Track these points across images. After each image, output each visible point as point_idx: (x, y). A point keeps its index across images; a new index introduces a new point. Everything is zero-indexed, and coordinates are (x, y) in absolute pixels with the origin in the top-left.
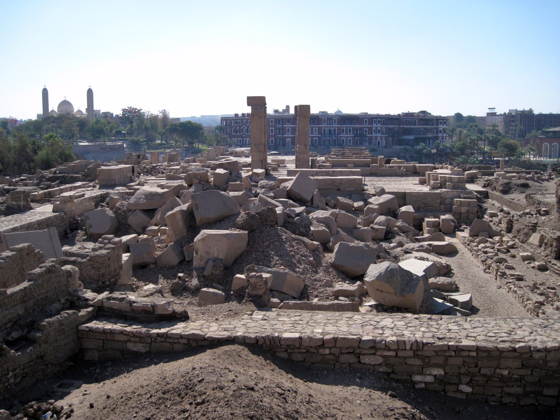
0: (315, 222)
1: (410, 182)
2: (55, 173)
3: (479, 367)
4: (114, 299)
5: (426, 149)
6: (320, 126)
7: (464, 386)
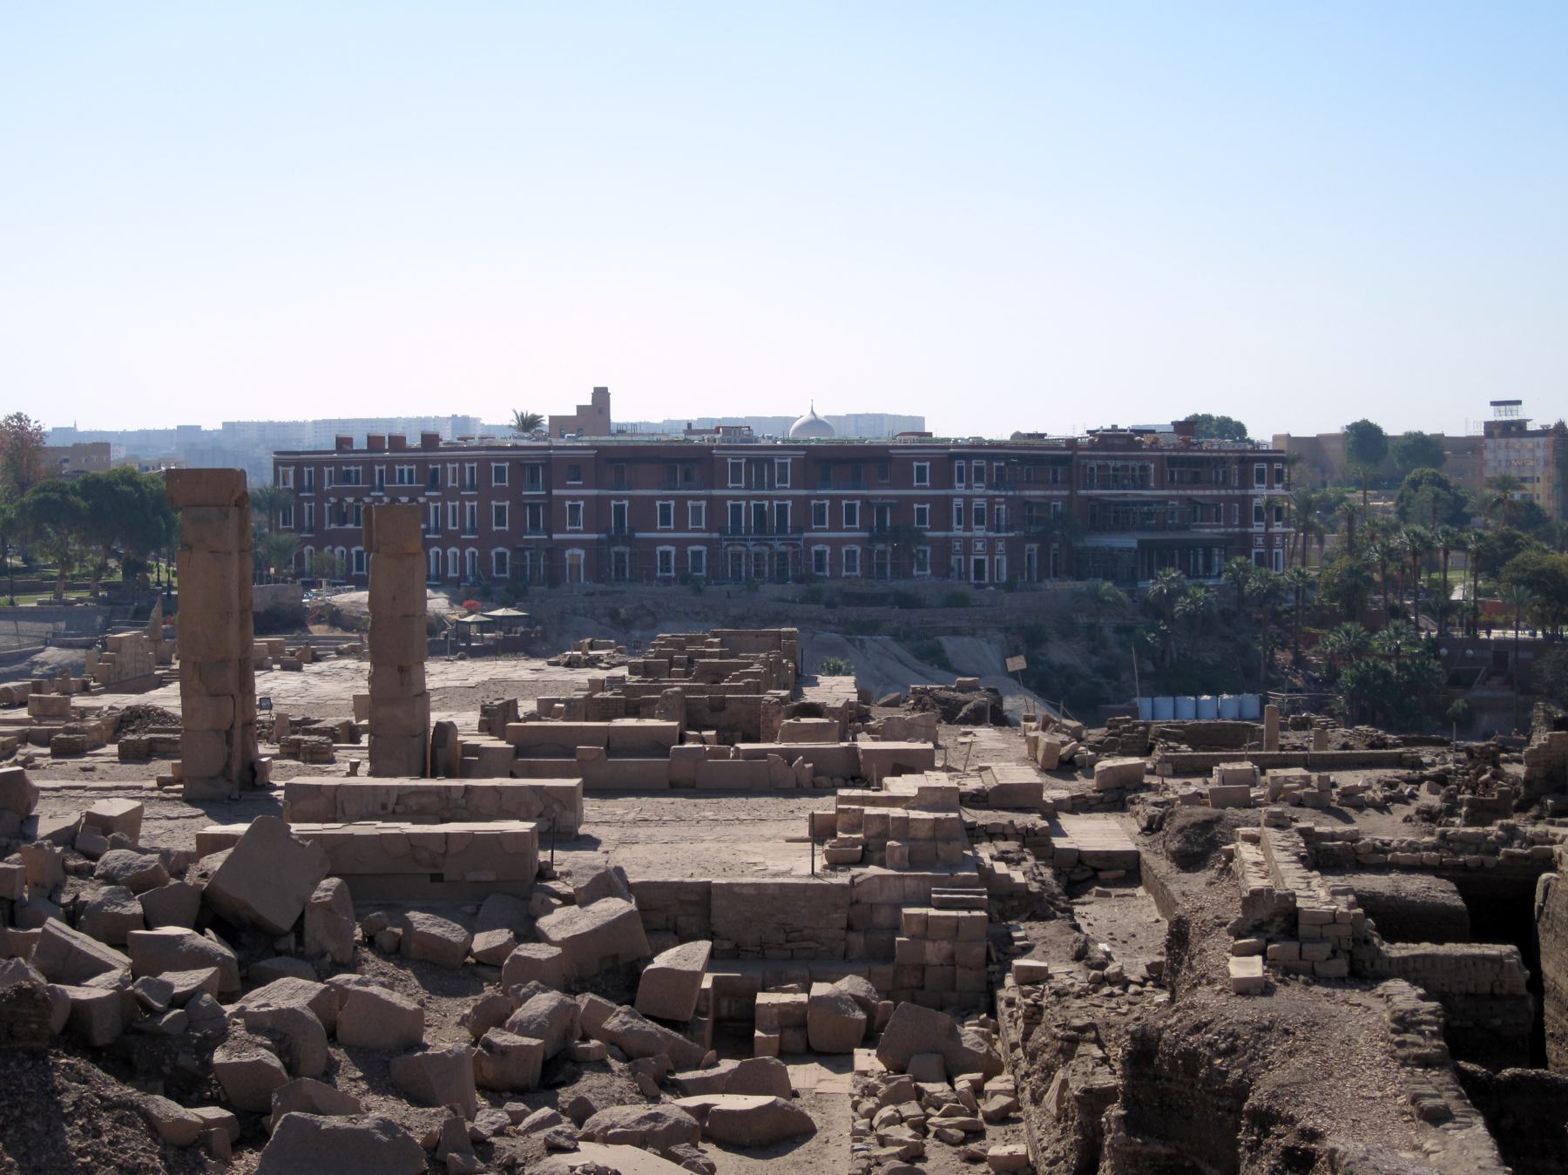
0: (239, 1030)
1: (767, 829)
5: (1186, 595)
6: (716, 492)
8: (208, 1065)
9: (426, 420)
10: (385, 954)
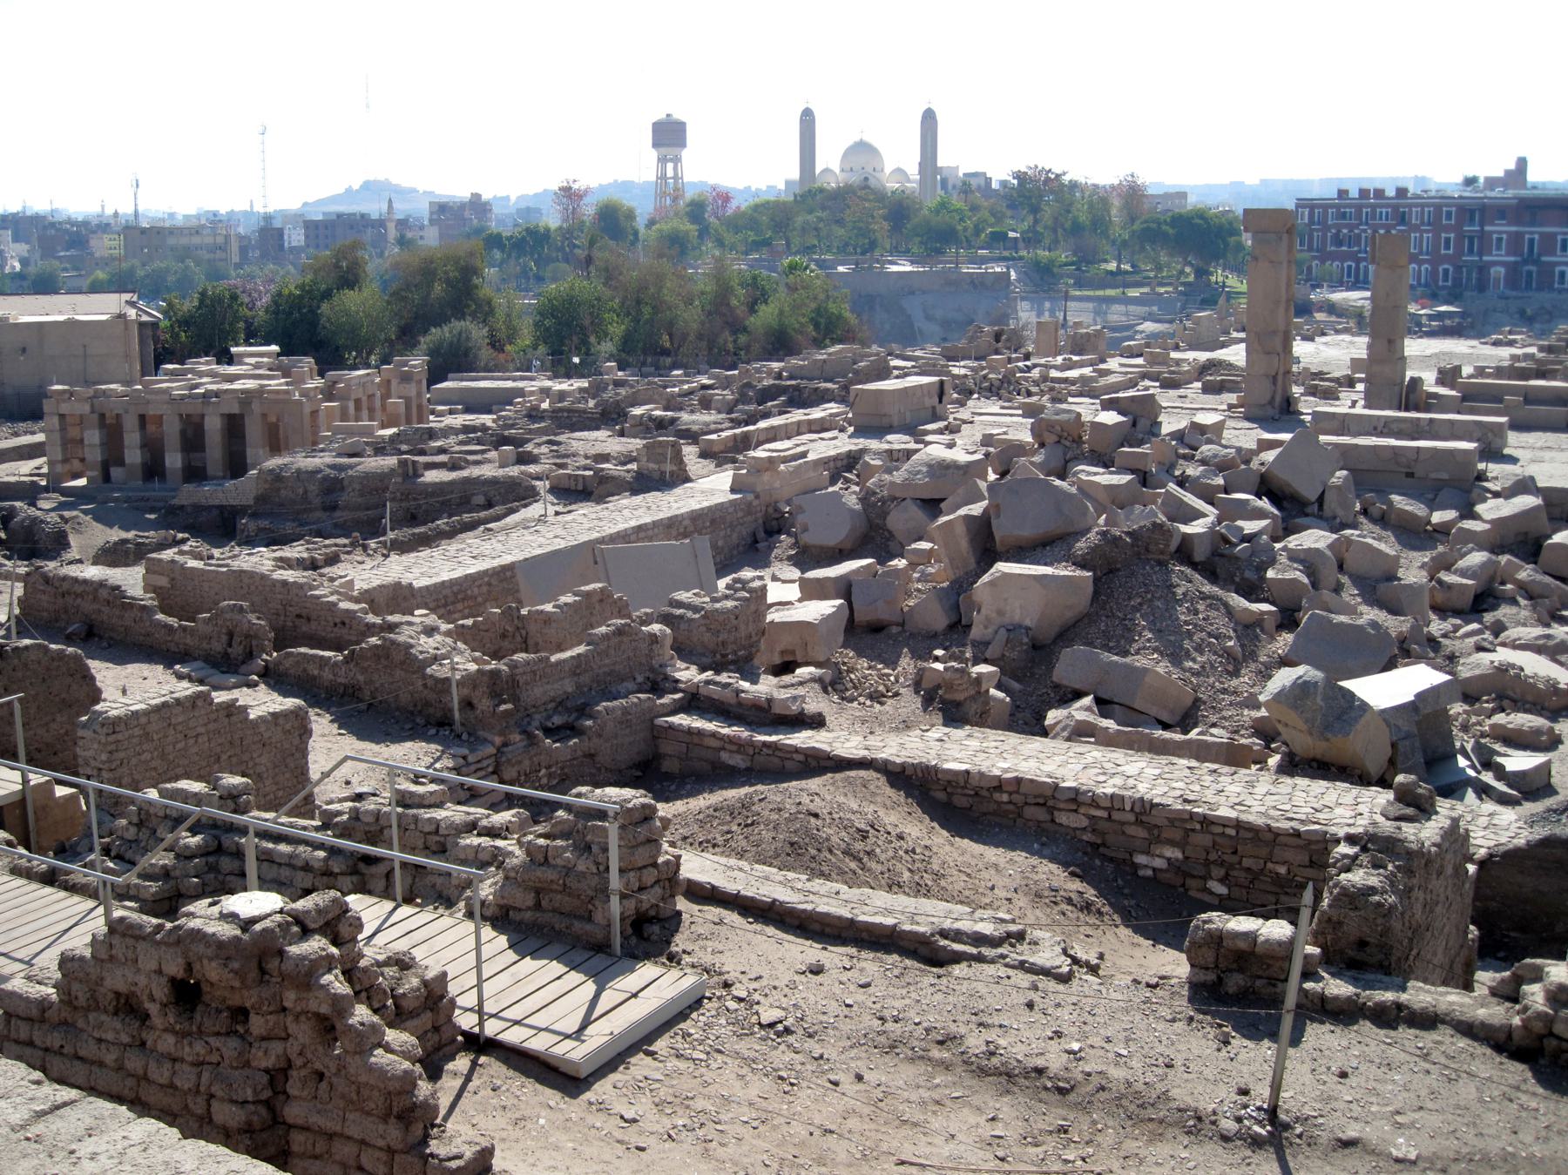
0: (1283, 559)
2: (779, 376)
3: (1239, 853)
4: (716, 683)
7: (1215, 883)
8: (1263, 579)
9: (1340, 180)
10: (1374, 521)
